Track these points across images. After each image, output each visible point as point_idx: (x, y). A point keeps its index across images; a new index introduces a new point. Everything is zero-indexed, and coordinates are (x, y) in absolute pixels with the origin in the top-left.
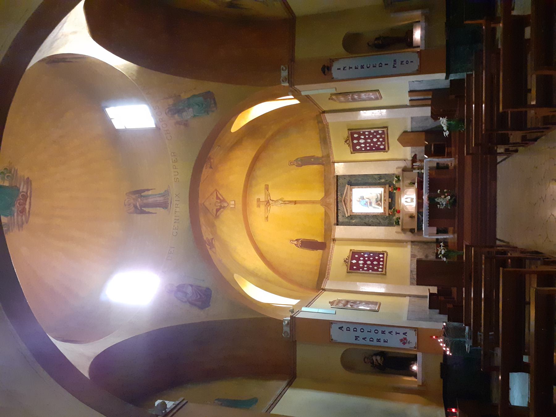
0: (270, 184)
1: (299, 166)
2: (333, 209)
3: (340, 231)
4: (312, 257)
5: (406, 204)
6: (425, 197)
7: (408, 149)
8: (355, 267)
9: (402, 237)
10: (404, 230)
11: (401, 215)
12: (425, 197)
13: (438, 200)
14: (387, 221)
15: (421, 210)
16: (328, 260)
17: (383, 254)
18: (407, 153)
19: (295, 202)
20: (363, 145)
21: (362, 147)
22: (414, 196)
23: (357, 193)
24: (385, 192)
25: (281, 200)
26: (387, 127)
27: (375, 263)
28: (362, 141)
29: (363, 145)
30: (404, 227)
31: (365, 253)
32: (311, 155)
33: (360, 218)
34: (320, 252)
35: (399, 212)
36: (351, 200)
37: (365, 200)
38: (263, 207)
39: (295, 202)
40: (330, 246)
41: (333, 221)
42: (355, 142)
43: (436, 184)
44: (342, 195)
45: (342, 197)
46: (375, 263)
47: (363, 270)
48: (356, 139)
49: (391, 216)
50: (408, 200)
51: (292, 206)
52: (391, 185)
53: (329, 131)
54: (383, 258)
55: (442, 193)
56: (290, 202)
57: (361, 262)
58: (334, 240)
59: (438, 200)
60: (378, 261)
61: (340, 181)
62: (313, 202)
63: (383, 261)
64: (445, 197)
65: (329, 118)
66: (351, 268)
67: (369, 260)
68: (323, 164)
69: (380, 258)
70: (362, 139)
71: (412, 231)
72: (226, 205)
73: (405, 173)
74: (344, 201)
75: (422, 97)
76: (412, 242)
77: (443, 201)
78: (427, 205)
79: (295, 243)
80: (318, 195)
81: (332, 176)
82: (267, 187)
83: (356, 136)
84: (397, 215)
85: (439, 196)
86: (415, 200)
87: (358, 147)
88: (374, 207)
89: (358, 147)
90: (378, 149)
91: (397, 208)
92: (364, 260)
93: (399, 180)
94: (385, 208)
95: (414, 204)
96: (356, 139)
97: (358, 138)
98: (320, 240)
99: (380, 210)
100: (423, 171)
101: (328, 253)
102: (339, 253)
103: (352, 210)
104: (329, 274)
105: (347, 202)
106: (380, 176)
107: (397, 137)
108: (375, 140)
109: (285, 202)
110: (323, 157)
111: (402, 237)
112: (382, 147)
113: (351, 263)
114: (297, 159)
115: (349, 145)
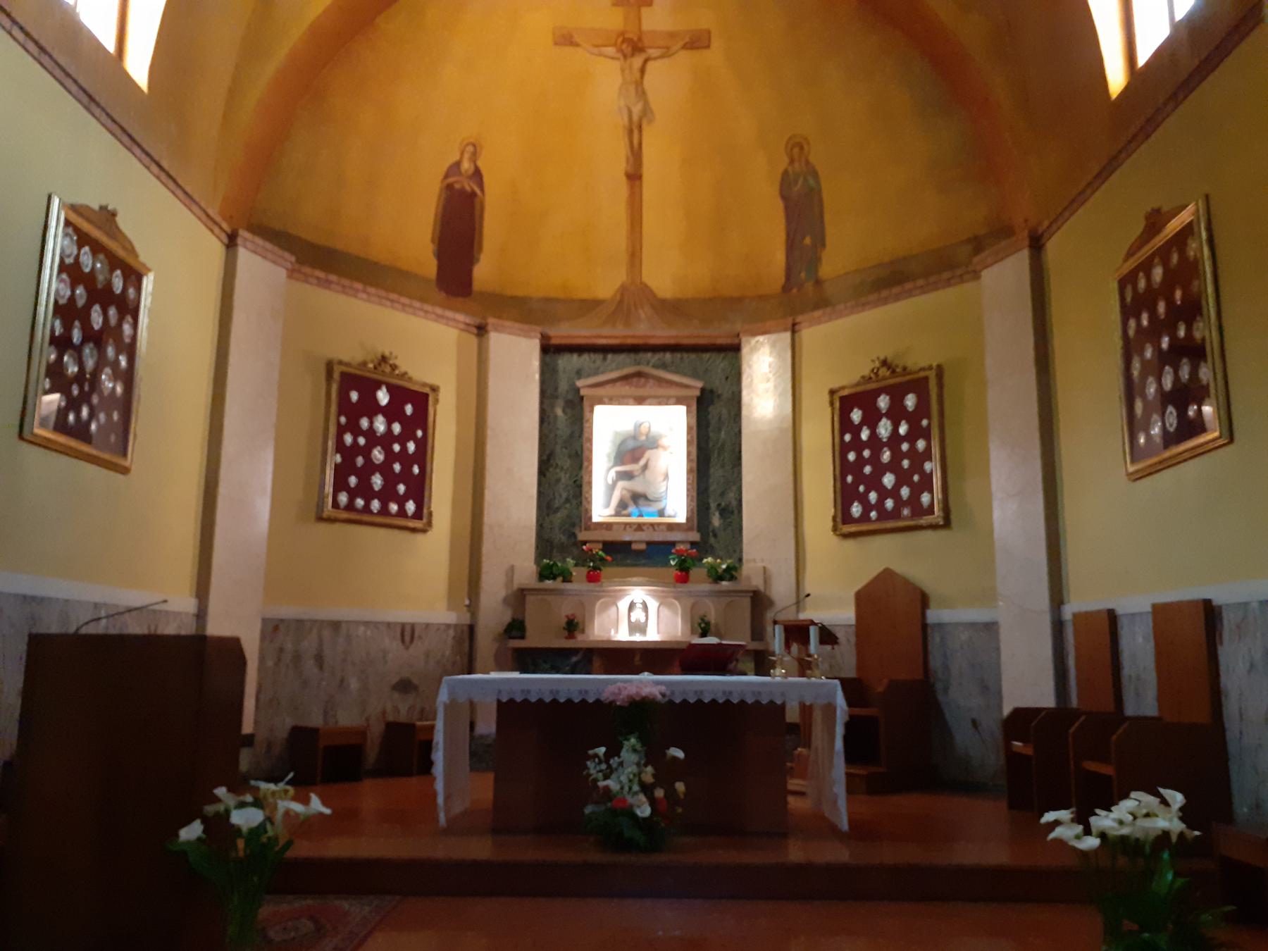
0: (714, 56)
1: (786, 183)
2: (606, 331)
3: (516, 359)
4: (413, 239)
5: (623, 605)
6: (647, 683)
7: (841, 614)
8: (354, 396)
9: (494, 591)
10: (519, 597)
11: (579, 585)
12: (647, 683)
13: (630, 755)
14: (560, 537)
15: (597, 662)
16: (387, 290)
17: (418, 515)
18: (834, 608)
19: (634, 177)
20: (865, 435)
21: (856, 431)
22: (653, 635)
23: (670, 424)
24: (672, 527)
25: (647, 111)
26: (947, 524)
27: (377, 481)
28: (884, 429)
29: (865, 435)
30: (530, 599)
31: (423, 445)
32: (829, 240)
33: (572, 435)
34: (428, 265)
35: (593, 578)
36: (640, 401)
37: (641, 448)
38: (614, 20)
39: (634, 177)
40: (457, 310)
41: (563, 332)
42: (883, 402)
43: (713, 741)
44: (664, 366)
45: (655, 366)
46: (377, 481)
47: (341, 430)
48: (897, 403)
49: (576, 549)
50: (638, 613)
51: (620, 166)
52: (701, 550)
53: (935, 287)
54: (402, 513)
55: (667, 772)
56: (636, 155)
57: (380, 425)
58: (481, 330)
59: (630, 755)
60: (387, 494)
61: (719, 363)
62: (635, 256)
63: (384, 511)
64: (646, 789)
65: (1006, 277)
66: (350, 380)
67: (390, 457)
68: (786, 288)
69: (401, 502)
70: (896, 427)
71: (516, 628)
72: (646, 425)
73: (746, 602)
74: (639, 375)
75: (1071, 662)
76: (472, 629)
77: (624, 775)
78: (606, 696)
79: (466, 166)
80: (665, 274)
81: (738, 327)
82: (698, 42)
83: (910, 401)
84: (579, 573)
85: (653, 754)
86: (638, 638)
87: (856, 416)
88: (612, 488)
89: (856, 416)
90: (845, 496)
91: (606, 571)
92: (389, 438)
93: (718, 578)
94: (607, 526)
95: (622, 635)
96: (897, 403)
97: (897, 413)
98: (484, 272)
99: (601, 508)
100: (780, 671)
101: (423, 300)
102: (426, 345)
103: (601, 402)
104: (326, 284)
105: (637, 388)
106: (732, 513)
107: (899, 568)
108: (888, 480)
109: (634, 130)
110: (818, 283)
111: (494, 591)
112: (856, 510)
113: (378, 385)
114: (815, 174)
115: (858, 384)
